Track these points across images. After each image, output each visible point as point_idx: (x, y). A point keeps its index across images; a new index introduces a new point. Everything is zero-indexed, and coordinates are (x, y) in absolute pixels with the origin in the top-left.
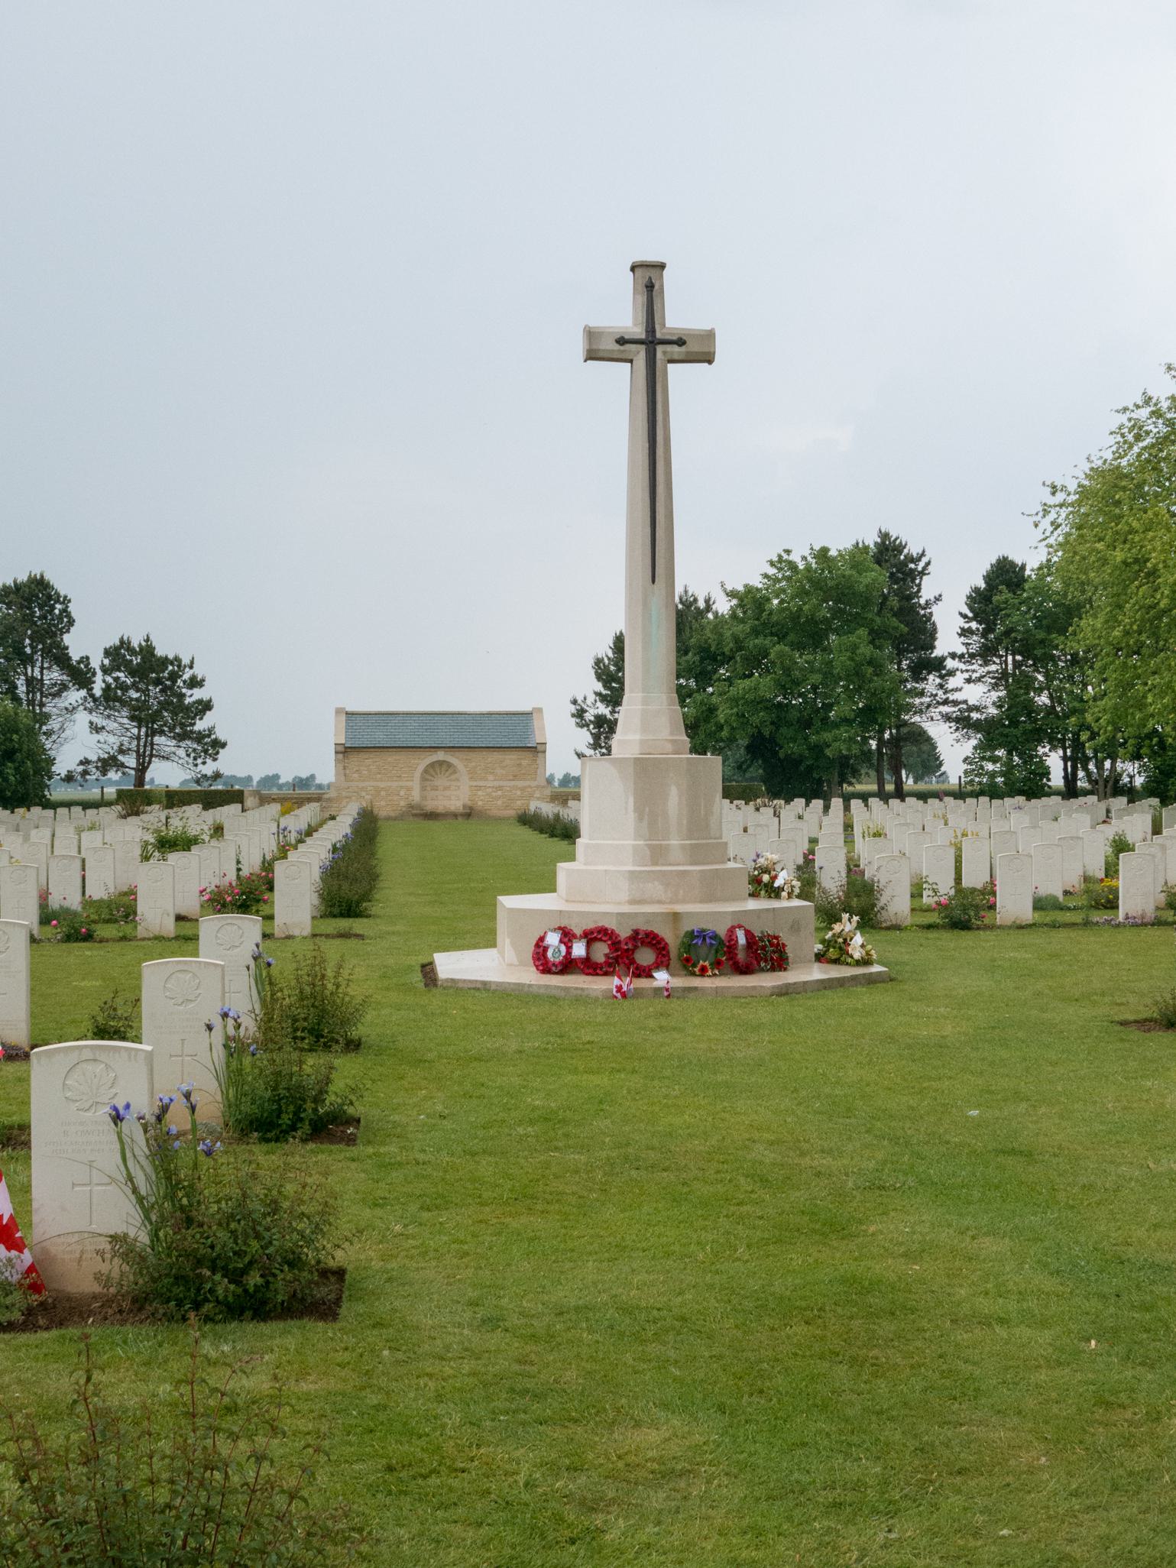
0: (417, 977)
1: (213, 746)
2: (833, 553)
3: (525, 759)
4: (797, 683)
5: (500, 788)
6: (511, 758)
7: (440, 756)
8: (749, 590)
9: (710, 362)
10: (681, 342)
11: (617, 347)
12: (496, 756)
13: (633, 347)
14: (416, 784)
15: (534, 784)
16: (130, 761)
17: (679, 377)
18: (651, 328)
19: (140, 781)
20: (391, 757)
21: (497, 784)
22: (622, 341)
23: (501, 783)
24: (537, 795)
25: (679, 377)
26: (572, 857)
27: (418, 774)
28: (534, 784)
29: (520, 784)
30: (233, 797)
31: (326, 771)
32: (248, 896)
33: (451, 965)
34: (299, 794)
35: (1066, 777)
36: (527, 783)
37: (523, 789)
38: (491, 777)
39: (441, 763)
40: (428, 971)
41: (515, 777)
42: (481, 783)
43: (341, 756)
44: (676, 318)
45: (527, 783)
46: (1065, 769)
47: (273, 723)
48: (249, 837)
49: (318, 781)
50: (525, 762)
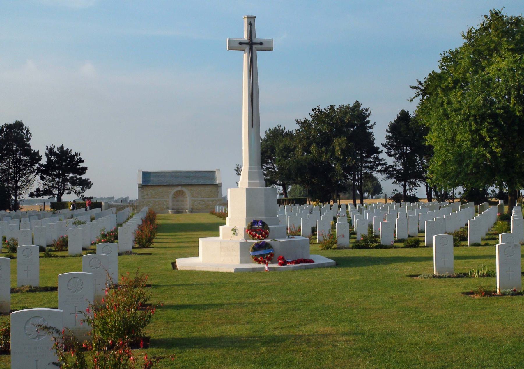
0: (171, 266)
1: (86, 184)
2: (336, 107)
3: (214, 189)
4: (318, 158)
5: (203, 201)
6: (208, 189)
7: (179, 188)
8: (306, 121)
9: (272, 50)
10: (261, 44)
11: (239, 45)
12: (202, 188)
13: (245, 45)
14: (170, 200)
15: (217, 199)
16: (56, 192)
17: (260, 55)
18: (251, 39)
19: (59, 199)
20: (160, 189)
21: (202, 199)
22: (241, 43)
23: (204, 199)
24: (218, 203)
25: (260, 55)
26: (225, 224)
27: (171, 196)
28: (217, 199)
29: (212, 199)
30: (98, 205)
31: (134, 195)
32: (112, 237)
33: (183, 264)
34: (121, 205)
35: (427, 194)
36: (214, 199)
37: (213, 201)
38: (200, 197)
39: (180, 191)
40: (174, 265)
41: (209, 196)
42: (196, 199)
43: (140, 189)
44: (259, 36)
45: (214, 199)
46: (427, 191)
47: (112, 176)
48: (107, 222)
49: (130, 199)
50: (213, 190)
